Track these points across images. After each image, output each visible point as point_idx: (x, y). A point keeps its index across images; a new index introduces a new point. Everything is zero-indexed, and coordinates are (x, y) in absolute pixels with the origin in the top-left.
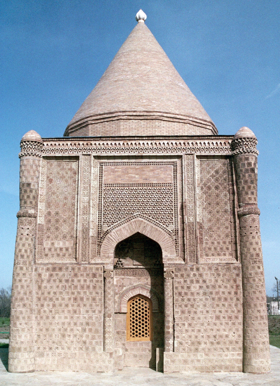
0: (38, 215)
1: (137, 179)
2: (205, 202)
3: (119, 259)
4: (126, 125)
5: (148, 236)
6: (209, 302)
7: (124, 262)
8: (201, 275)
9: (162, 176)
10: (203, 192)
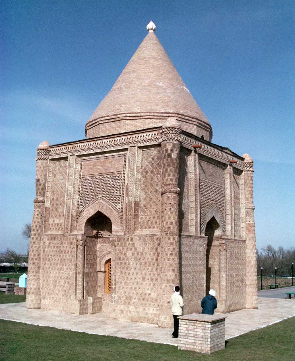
0: (45, 201)
1: (101, 169)
2: (143, 184)
3: (98, 231)
4: (103, 127)
5: (104, 214)
6: (139, 266)
7: (103, 233)
8: (133, 244)
9: (117, 166)
10: (143, 177)
